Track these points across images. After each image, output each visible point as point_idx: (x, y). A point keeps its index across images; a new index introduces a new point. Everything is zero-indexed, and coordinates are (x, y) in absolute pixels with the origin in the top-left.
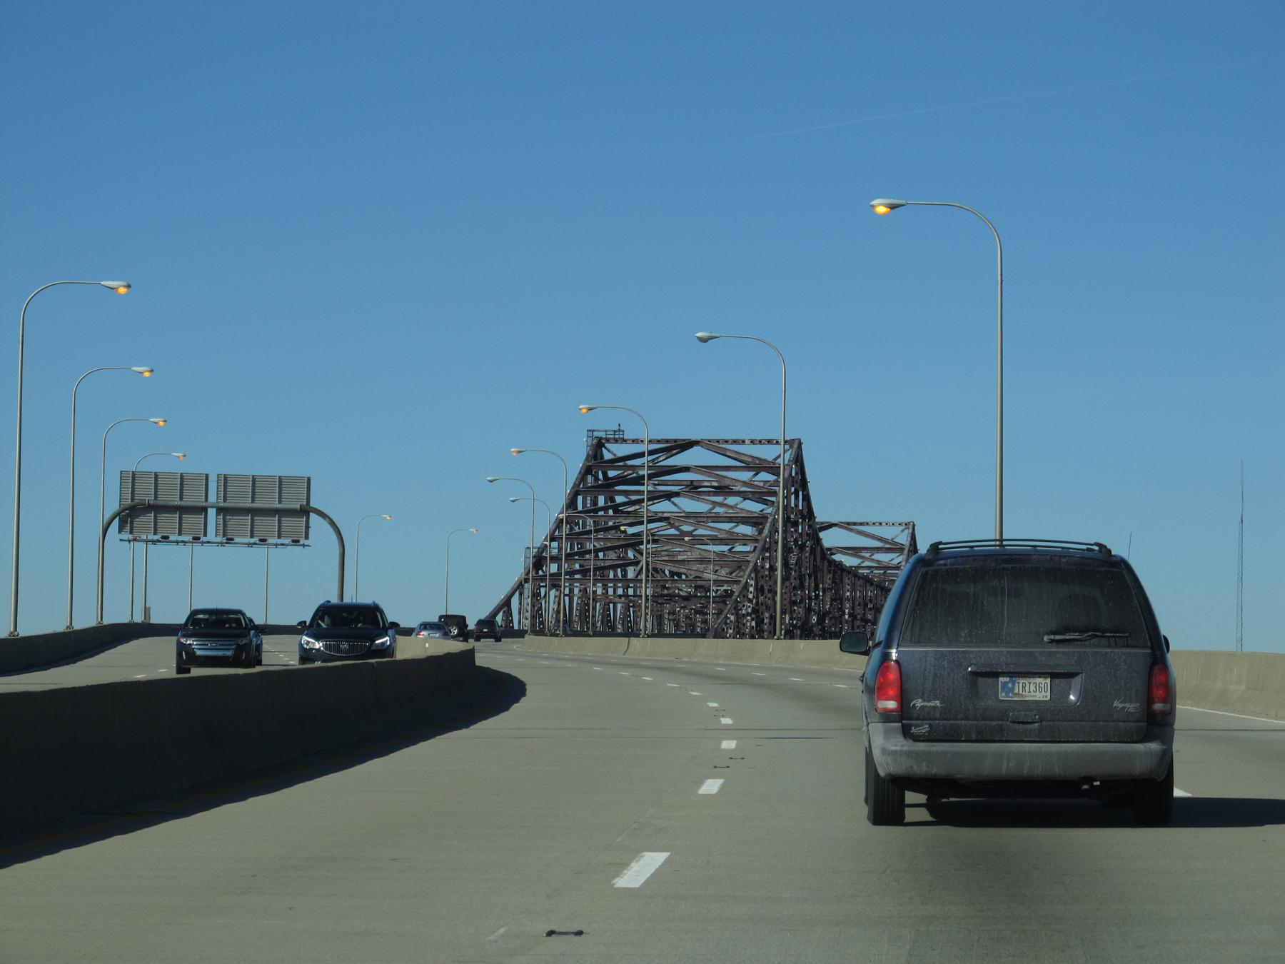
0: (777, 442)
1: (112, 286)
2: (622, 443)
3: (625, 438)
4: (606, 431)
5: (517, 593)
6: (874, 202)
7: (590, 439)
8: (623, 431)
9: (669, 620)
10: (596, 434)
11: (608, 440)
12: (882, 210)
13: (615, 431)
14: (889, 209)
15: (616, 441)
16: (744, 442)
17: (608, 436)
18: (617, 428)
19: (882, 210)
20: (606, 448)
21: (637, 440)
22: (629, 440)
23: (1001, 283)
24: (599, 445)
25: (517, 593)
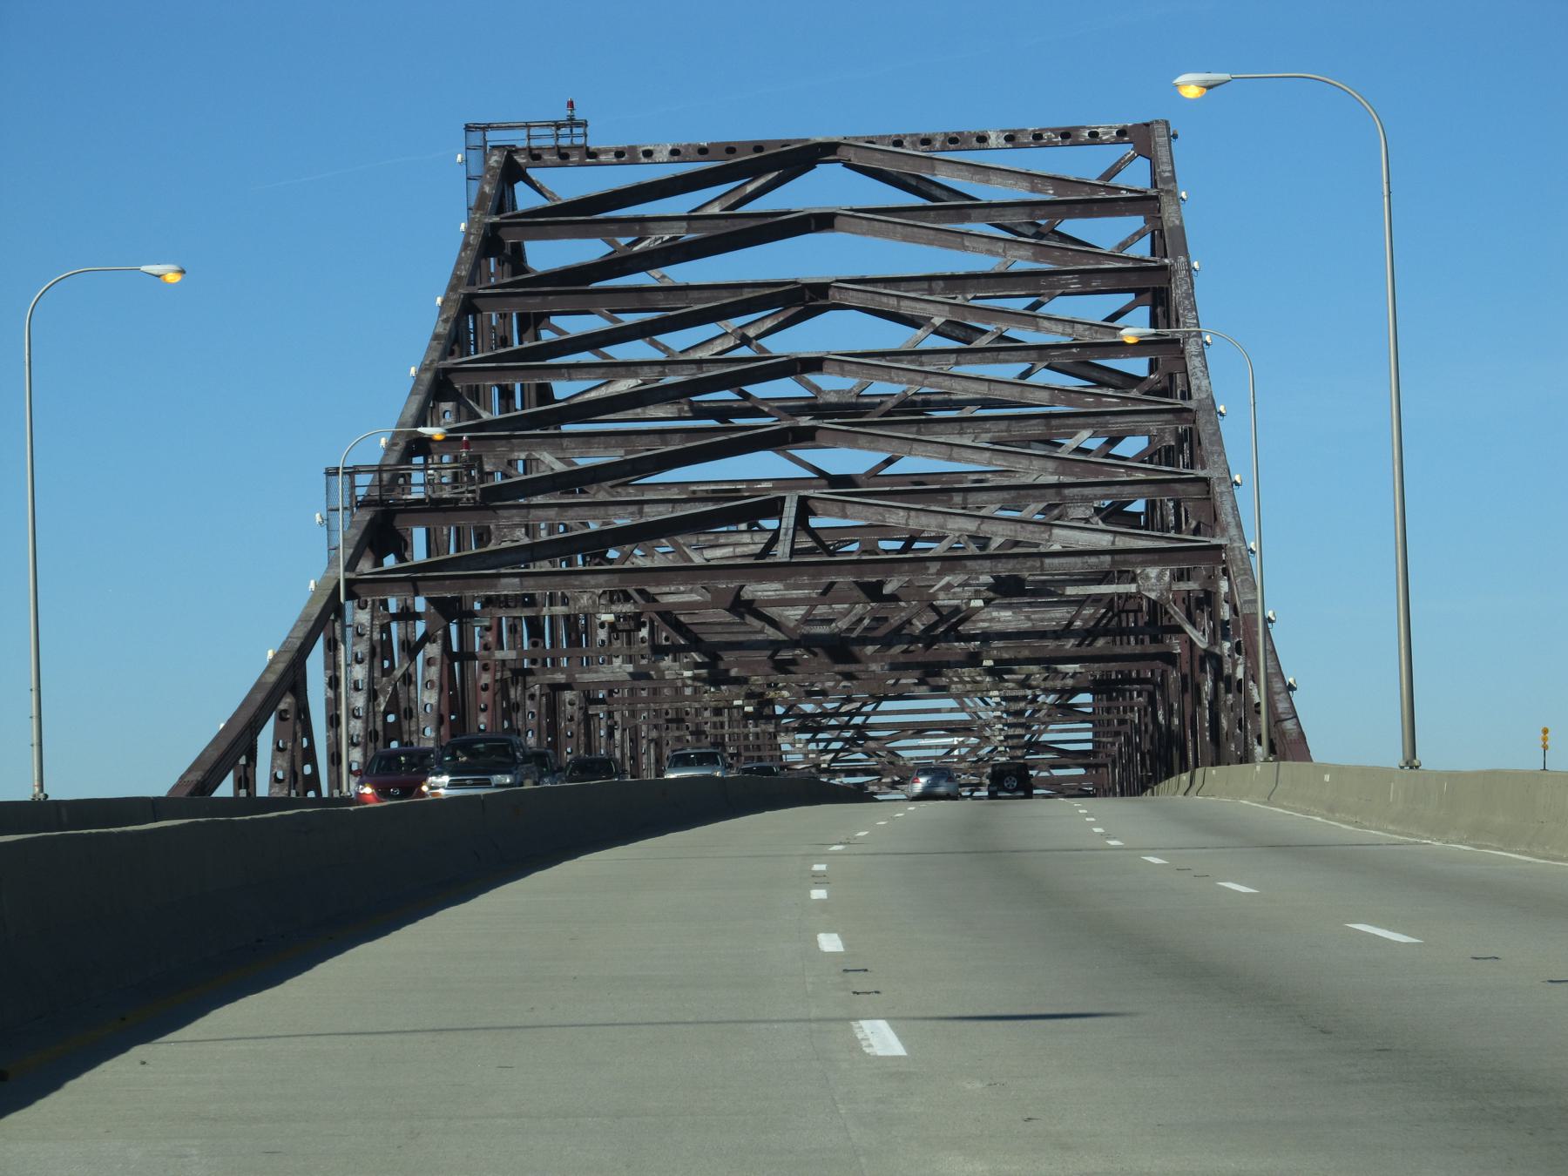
0: (1094, 135)
1: (156, 272)
2: (581, 164)
3: (593, 145)
4: (528, 126)
5: (319, 647)
6: (1179, 80)
7: (476, 156)
8: (584, 124)
9: (650, 741)
10: (494, 137)
11: (535, 156)
12: (1191, 92)
13: (558, 126)
14: (1205, 90)
15: (563, 156)
16: (982, 139)
17: (534, 143)
18: (562, 115)
19: (1191, 92)
20: (531, 183)
21: (633, 149)
22: (606, 151)
23: (1389, 196)
24: (511, 172)
25: (319, 647)
